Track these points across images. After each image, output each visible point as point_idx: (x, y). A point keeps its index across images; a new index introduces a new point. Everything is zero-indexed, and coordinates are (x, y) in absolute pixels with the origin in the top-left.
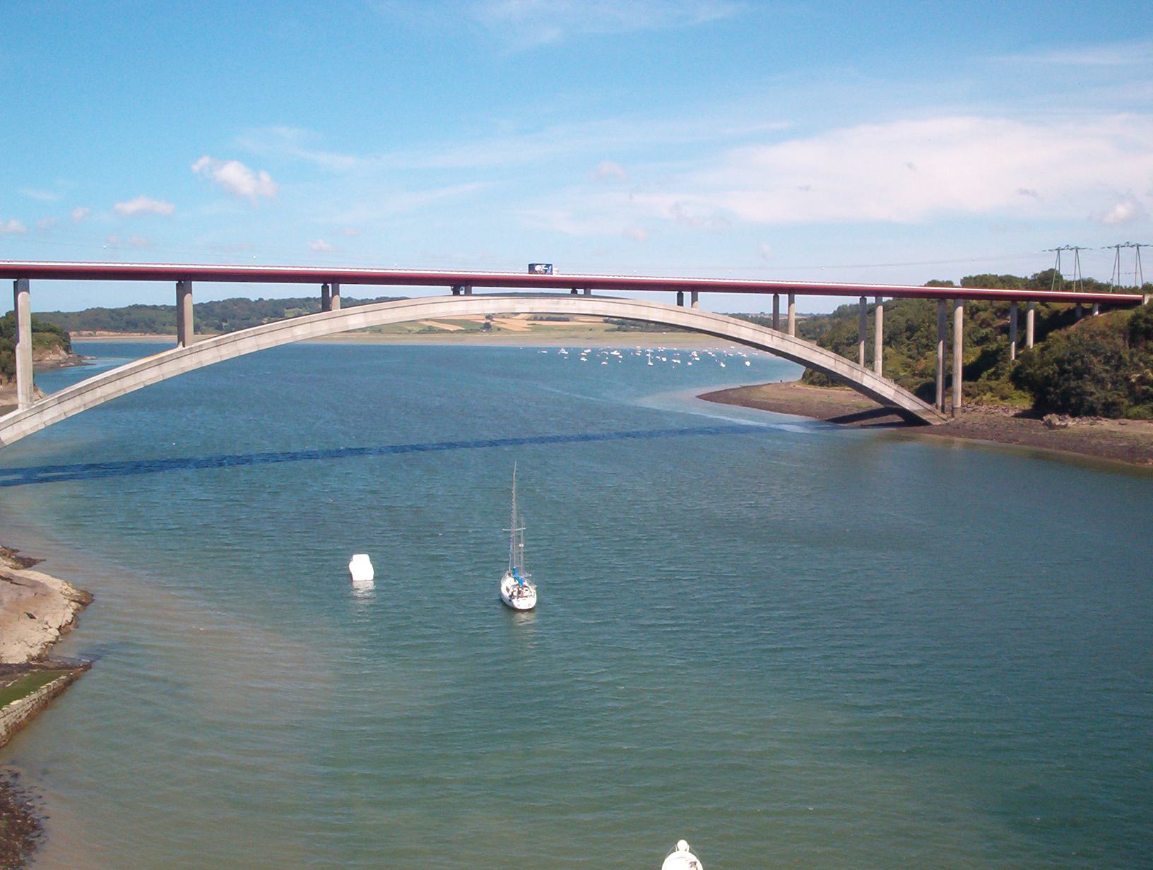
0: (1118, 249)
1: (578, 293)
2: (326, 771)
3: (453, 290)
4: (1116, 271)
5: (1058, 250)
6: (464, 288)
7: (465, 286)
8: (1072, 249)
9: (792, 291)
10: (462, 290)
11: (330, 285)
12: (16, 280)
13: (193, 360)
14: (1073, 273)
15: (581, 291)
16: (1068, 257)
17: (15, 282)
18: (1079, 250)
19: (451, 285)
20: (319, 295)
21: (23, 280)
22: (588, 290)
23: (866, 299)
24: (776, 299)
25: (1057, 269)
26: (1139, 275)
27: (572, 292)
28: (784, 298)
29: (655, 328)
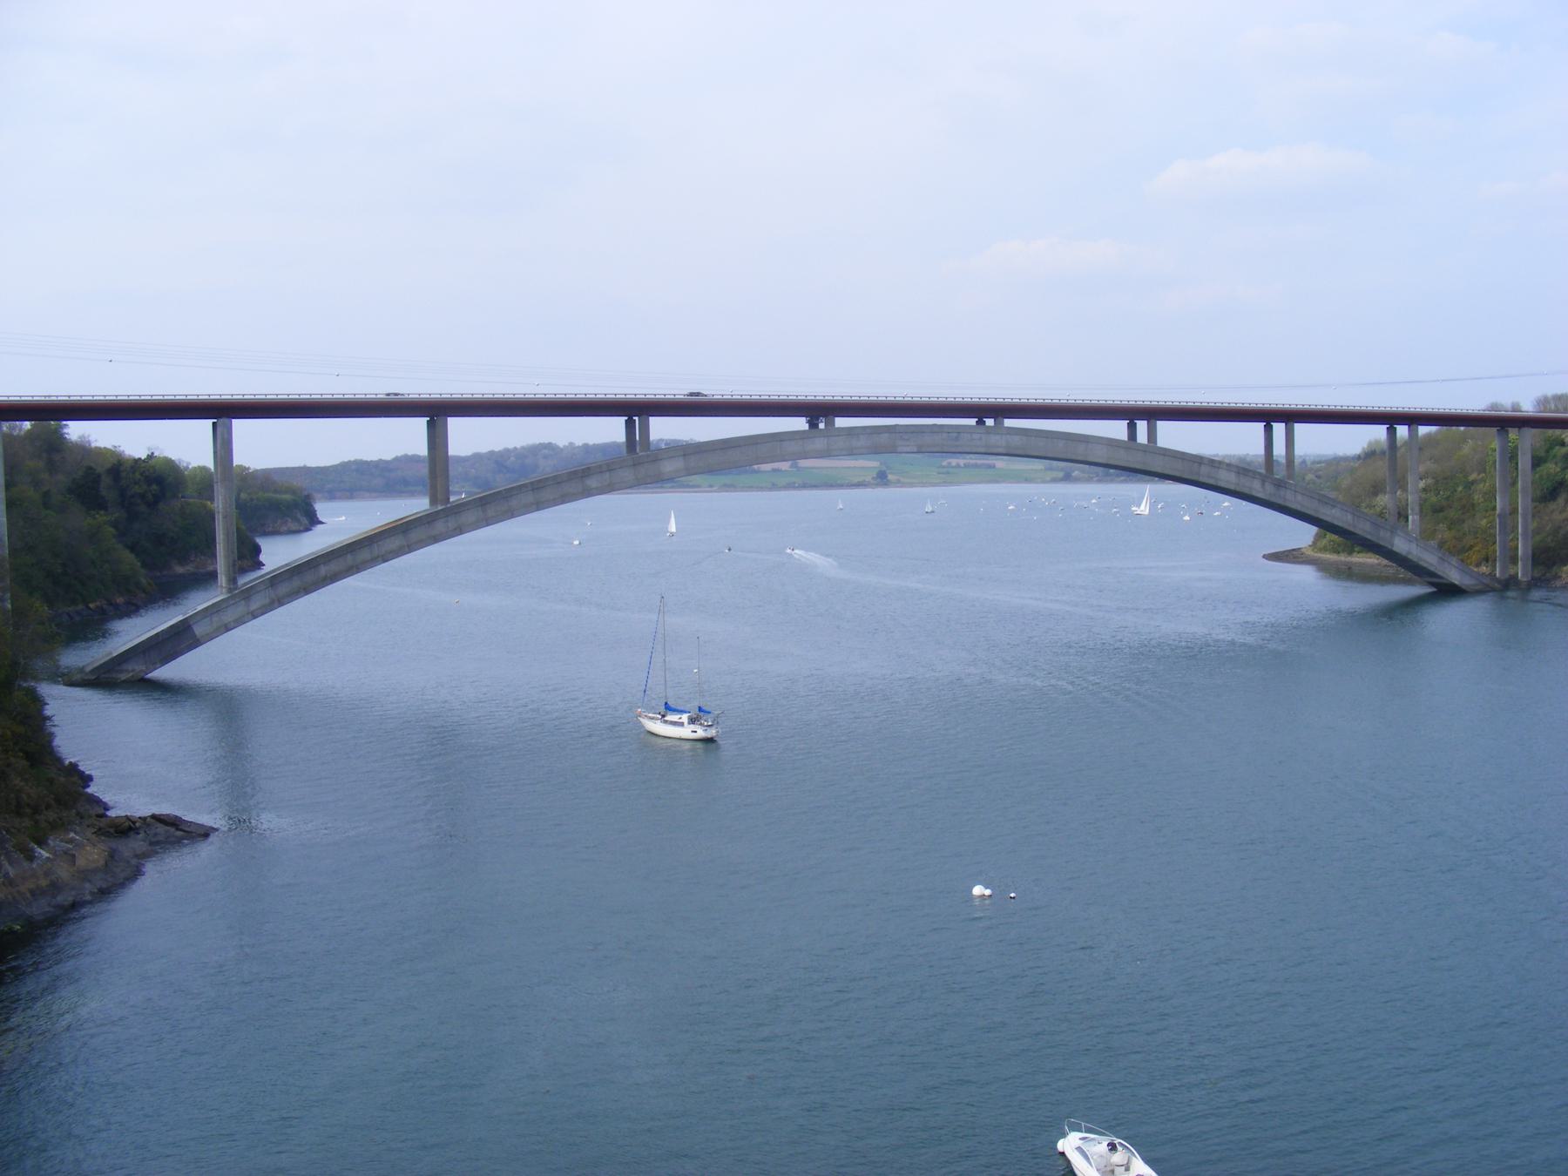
1: (987, 424)
3: (808, 422)
7: (825, 416)
9: (1292, 417)
10: (822, 422)
11: (636, 418)
12: (215, 420)
13: (450, 525)
15: (990, 422)
17: (214, 423)
19: (807, 417)
20: (422, 449)
21: (226, 420)
22: (1000, 419)
23: (1395, 428)
24: (1268, 431)
28: (1279, 429)
29: (1204, 469)
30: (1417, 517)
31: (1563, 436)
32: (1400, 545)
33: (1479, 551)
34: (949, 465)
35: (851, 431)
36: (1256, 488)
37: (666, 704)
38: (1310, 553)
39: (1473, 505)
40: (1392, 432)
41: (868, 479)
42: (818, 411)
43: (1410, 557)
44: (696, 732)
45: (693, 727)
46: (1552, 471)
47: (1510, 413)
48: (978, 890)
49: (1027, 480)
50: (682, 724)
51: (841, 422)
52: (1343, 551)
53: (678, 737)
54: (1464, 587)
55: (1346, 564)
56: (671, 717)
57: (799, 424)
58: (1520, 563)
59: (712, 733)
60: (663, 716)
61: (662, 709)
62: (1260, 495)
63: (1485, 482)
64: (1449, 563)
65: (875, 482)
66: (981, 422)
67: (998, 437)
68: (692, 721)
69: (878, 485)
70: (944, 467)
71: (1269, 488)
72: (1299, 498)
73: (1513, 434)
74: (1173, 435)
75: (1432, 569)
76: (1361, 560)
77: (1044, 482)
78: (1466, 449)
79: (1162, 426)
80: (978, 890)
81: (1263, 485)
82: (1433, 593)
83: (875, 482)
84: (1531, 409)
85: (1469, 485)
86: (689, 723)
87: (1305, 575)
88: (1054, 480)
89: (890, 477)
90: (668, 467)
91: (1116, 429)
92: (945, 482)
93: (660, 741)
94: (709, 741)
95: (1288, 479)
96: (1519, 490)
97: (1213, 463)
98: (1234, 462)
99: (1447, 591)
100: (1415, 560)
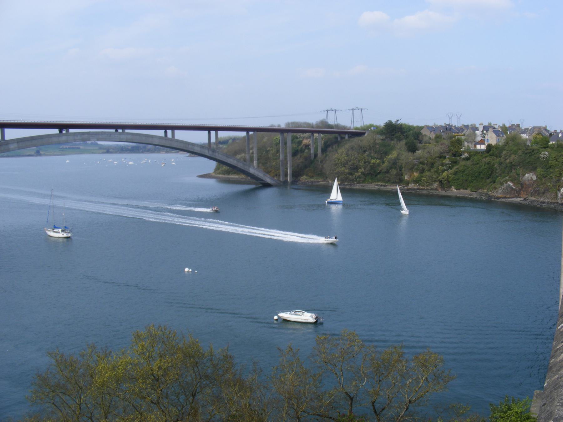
0: (353, 111)
2: (555, 377)
3: (59, 131)
4: (353, 120)
5: (353, 110)
6: (65, 130)
8: (333, 110)
9: (217, 129)
10: (64, 131)
14: (334, 121)
15: (120, 131)
16: (331, 114)
18: (336, 111)
22: (124, 130)
23: (249, 133)
24: (209, 133)
25: (327, 121)
26: (362, 122)
27: (115, 131)
28: (213, 133)
30: (256, 162)
31: (297, 135)
32: (252, 171)
33: (274, 173)
34: (63, 147)
35: (75, 134)
36: (206, 152)
37: (54, 226)
38: (214, 174)
39: (269, 158)
40: (248, 133)
41: (33, 153)
42: (61, 127)
43: (255, 174)
44: (63, 235)
45: (63, 233)
46: (294, 147)
47: (277, 128)
48: (187, 269)
49: (93, 153)
50: (59, 232)
51: (71, 131)
52: (226, 174)
53: (58, 237)
54: (271, 184)
55: (228, 178)
56: (56, 230)
57: (56, 131)
58: (288, 176)
59: (69, 235)
60: (53, 230)
61: (53, 228)
62: (208, 155)
63: (273, 150)
64: (267, 176)
65: (35, 154)
66: (117, 131)
67: (123, 136)
68: (63, 231)
69: (37, 156)
70: (61, 148)
71: (210, 152)
72: (220, 156)
73: (286, 134)
74: (180, 135)
75: (261, 178)
76: (232, 177)
77: (99, 153)
78: (265, 139)
79: (177, 132)
80: (187, 269)
81: (209, 151)
82: (261, 186)
83: (35, 154)
84: (284, 126)
85: (267, 152)
86: (61, 232)
87: (212, 182)
88: (103, 153)
89: (41, 152)
90: (12, 146)
91: (161, 133)
92: (62, 154)
93: (53, 238)
94: (69, 237)
95: (217, 149)
96: (288, 152)
97: (193, 144)
98: (199, 144)
99: (266, 185)
100: (256, 175)
